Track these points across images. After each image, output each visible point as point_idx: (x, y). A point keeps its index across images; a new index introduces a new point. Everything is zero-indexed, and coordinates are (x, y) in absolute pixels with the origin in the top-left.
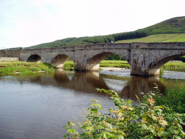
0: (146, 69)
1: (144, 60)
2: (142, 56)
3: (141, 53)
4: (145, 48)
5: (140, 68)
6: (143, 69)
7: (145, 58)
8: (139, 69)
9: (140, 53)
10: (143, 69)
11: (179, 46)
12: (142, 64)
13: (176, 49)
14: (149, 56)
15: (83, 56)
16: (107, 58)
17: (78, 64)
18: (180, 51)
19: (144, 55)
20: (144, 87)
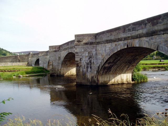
0: (93, 75)
1: (90, 62)
2: (87, 55)
3: (85, 50)
4: (91, 43)
5: (84, 74)
6: (89, 76)
7: (91, 57)
8: (83, 75)
9: (83, 50)
10: (89, 76)
11: (124, 32)
12: (87, 67)
13: (120, 40)
14: (97, 55)
15: (58, 58)
16: (163, 58)
17: (53, 68)
18: (126, 42)
19: (89, 53)
20: (92, 103)
